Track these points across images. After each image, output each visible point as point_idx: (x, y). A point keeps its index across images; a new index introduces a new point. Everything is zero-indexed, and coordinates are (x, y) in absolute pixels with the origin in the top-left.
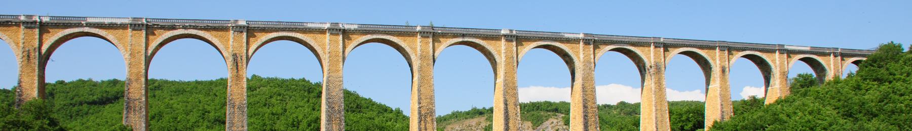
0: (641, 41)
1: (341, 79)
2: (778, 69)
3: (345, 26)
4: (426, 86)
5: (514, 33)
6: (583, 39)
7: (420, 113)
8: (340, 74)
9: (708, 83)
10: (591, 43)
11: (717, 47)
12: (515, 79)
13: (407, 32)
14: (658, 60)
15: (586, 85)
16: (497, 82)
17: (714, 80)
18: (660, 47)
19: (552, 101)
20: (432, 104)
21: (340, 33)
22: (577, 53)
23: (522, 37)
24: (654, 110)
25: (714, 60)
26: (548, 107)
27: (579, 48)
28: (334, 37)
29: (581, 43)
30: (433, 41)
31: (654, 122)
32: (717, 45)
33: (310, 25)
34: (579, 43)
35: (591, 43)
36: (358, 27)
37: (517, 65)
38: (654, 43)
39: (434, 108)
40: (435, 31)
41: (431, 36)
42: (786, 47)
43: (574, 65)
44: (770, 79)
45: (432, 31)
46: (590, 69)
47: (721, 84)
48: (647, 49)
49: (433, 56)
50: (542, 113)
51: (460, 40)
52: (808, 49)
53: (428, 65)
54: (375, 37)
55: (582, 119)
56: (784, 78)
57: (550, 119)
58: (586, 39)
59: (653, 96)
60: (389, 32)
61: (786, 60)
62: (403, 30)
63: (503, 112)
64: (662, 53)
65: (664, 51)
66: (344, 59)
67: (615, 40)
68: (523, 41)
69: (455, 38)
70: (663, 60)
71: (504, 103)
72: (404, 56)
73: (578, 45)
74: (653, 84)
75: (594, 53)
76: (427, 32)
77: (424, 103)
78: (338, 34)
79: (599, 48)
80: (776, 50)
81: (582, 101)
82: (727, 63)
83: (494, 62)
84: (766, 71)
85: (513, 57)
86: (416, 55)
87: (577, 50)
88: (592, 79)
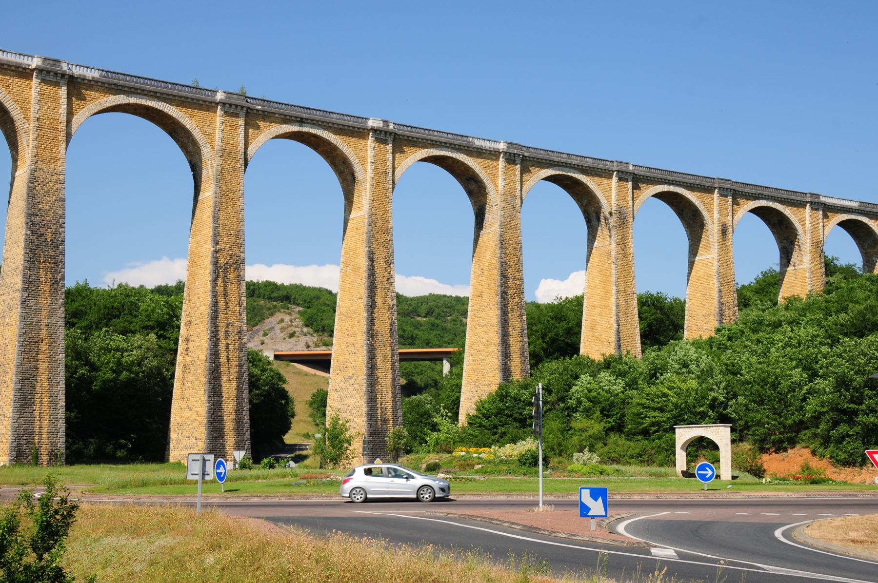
0: (598, 166)
1: (61, 177)
2: (809, 236)
3: (74, 69)
4: (229, 210)
5: (391, 127)
6: (506, 153)
7: (215, 262)
8: (61, 166)
9: (693, 251)
10: (518, 160)
11: (715, 188)
12: (389, 215)
13: (198, 100)
14: (622, 203)
15: (506, 236)
16: (351, 216)
17: (708, 248)
18: (627, 180)
19: (279, 282)
20: (240, 246)
21: (62, 81)
22: (494, 176)
23: (403, 136)
24: (614, 292)
25: (710, 211)
26: (272, 292)
27: (496, 168)
28: (50, 90)
29: (501, 160)
30: (246, 125)
31: (614, 312)
32: (716, 185)
34: (497, 159)
35: (518, 160)
36: (101, 76)
37: (393, 188)
38: (618, 171)
39: (242, 255)
40: (252, 106)
41: (242, 113)
42: (822, 199)
43: (486, 199)
45: (244, 103)
46: (514, 208)
47: (720, 255)
48: (605, 181)
49: (245, 153)
50: (262, 303)
51: (295, 128)
52: (855, 205)
53: (235, 169)
54: (133, 100)
55: (498, 299)
56: (816, 252)
57: (278, 314)
58: (510, 154)
59: (613, 266)
60: (162, 94)
61: (821, 221)
62: (189, 95)
63: (365, 275)
64: (630, 191)
65: (633, 188)
66: (69, 136)
67: (556, 159)
70: (631, 203)
71: (369, 258)
72: (183, 147)
73: (495, 163)
74: (613, 246)
75: (521, 181)
76: (237, 106)
77: (224, 245)
78: (57, 84)
79: (529, 171)
80: (807, 202)
81: (498, 266)
82: (730, 218)
83: (349, 178)
84: (786, 239)
85: (386, 173)
86: (213, 147)
87: (494, 172)
88: (516, 227)
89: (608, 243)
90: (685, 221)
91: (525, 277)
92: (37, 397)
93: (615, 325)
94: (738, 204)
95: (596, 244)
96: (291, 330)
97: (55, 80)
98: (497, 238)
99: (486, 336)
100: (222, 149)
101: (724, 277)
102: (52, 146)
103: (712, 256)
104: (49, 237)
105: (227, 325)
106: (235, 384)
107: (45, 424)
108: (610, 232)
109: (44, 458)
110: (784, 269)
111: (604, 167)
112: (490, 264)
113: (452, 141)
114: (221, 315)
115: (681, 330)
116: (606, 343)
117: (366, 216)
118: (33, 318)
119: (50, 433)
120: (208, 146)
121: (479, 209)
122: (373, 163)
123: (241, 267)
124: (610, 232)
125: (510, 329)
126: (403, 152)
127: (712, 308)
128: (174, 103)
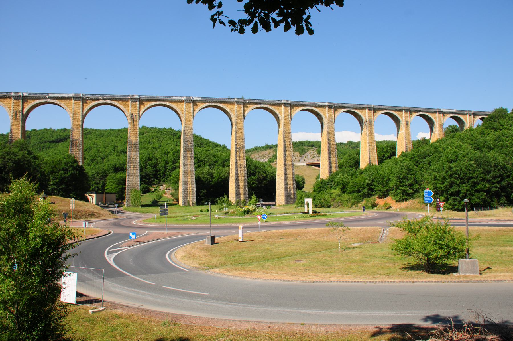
0: (361, 107)
2: (438, 122)
4: (239, 132)
5: (289, 102)
7: (236, 147)
8: (192, 125)
9: (398, 130)
10: (333, 108)
14: (370, 118)
15: (330, 131)
17: (402, 129)
18: (371, 110)
20: (243, 142)
22: (325, 113)
24: (368, 146)
25: (402, 117)
28: (188, 105)
29: (327, 108)
30: (243, 107)
31: (368, 152)
34: (326, 108)
35: (333, 108)
38: (368, 108)
40: (245, 101)
42: (442, 110)
45: (243, 101)
47: (405, 131)
48: (364, 111)
49: (244, 115)
50: (305, 147)
51: (259, 106)
52: (454, 111)
53: (241, 120)
54: (211, 104)
55: (327, 151)
57: (310, 151)
59: (367, 138)
61: (442, 117)
62: (226, 101)
63: (283, 147)
64: (373, 113)
65: (374, 113)
67: (346, 106)
70: (373, 117)
72: (227, 115)
74: (367, 131)
76: (240, 102)
78: (190, 103)
79: (337, 111)
81: (327, 141)
82: (409, 119)
83: (278, 118)
84: (431, 124)
85: (288, 116)
86: (234, 114)
88: (333, 128)
92: (188, 188)
93: (368, 156)
94: (412, 114)
95: (363, 131)
96: (313, 156)
98: (327, 132)
100: (237, 115)
101: (407, 138)
104: (189, 145)
105: (240, 165)
106: (243, 182)
107: (191, 195)
109: (191, 204)
111: (363, 107)
112: (325, 140)
113: (310, 104)
114: (238, 162)
115: (117, 197)
118: (186, 167)
119: (192, 197)
120: (233, 114)
125: (332, 160)
126: (294, 109)
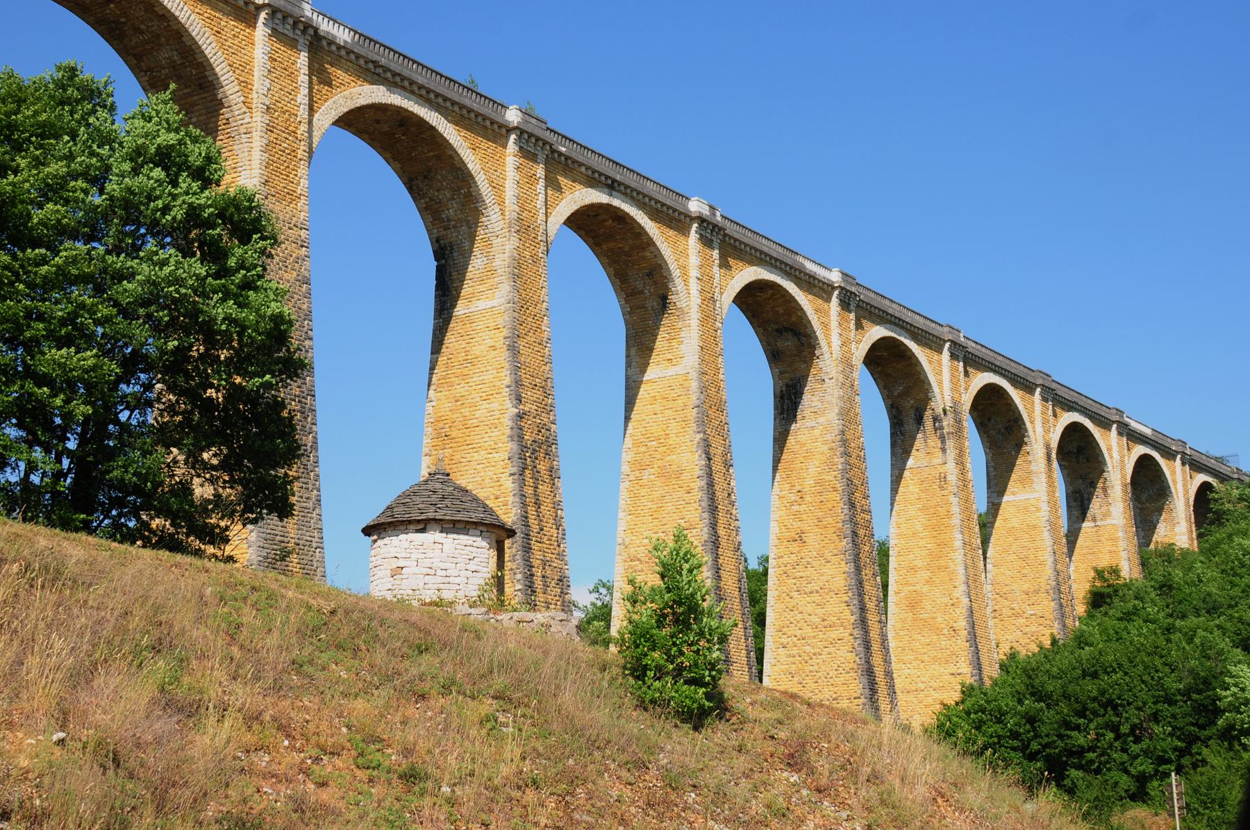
4: (531, 338)
17: (1027, 481)
28: (284, 52)
33: (810, 267)
44: (1090, 500)
68: (865, 318)
69: (591, 187)
72: (431, 211)
83: (653, 304)
84: (1083, 478)
89: (940, 461)
90: (988, 437)
91: (873, 508)
95: (910, 463)
97: (291, 35)
98: (833, 435)
99: (820, 611)
102: (288, 167)
103: (1036, 495)
108: (943, 442)
110: (1076, 526)
112: (819, 483)
114: (535, 546)
116: (945, 631)
117: (694, 375)
120: (497, 208)
121: (787, 385)
122: (699, 279)
123: (554, 450)
124: (943, 442)
127: (1042, 580)
128: (450, 118)
